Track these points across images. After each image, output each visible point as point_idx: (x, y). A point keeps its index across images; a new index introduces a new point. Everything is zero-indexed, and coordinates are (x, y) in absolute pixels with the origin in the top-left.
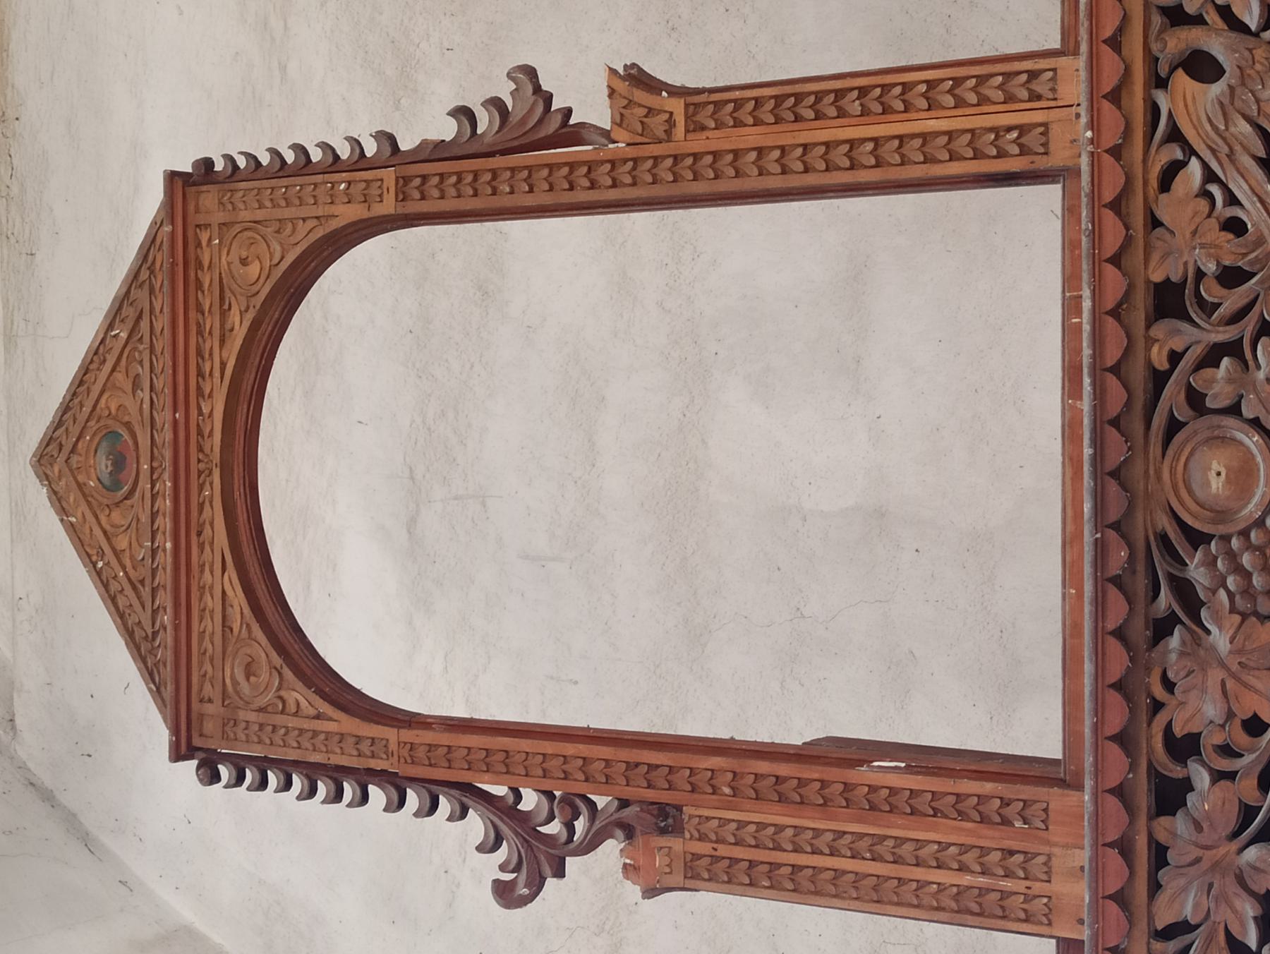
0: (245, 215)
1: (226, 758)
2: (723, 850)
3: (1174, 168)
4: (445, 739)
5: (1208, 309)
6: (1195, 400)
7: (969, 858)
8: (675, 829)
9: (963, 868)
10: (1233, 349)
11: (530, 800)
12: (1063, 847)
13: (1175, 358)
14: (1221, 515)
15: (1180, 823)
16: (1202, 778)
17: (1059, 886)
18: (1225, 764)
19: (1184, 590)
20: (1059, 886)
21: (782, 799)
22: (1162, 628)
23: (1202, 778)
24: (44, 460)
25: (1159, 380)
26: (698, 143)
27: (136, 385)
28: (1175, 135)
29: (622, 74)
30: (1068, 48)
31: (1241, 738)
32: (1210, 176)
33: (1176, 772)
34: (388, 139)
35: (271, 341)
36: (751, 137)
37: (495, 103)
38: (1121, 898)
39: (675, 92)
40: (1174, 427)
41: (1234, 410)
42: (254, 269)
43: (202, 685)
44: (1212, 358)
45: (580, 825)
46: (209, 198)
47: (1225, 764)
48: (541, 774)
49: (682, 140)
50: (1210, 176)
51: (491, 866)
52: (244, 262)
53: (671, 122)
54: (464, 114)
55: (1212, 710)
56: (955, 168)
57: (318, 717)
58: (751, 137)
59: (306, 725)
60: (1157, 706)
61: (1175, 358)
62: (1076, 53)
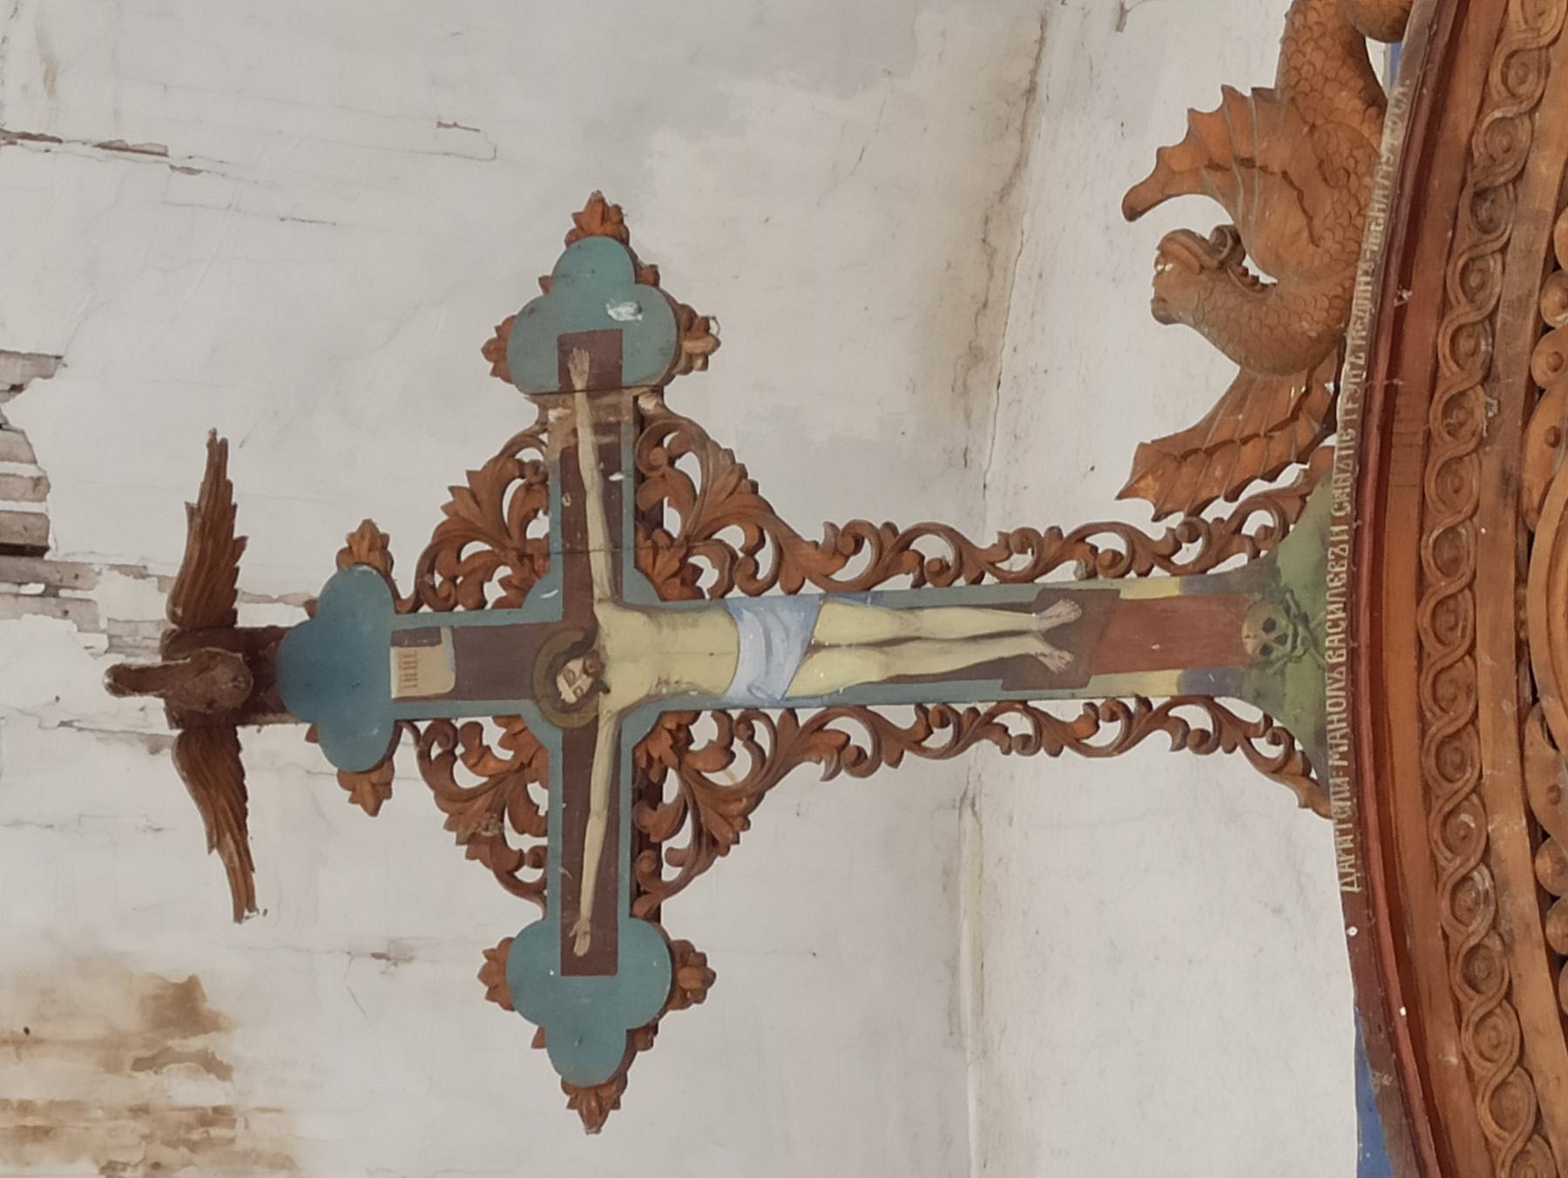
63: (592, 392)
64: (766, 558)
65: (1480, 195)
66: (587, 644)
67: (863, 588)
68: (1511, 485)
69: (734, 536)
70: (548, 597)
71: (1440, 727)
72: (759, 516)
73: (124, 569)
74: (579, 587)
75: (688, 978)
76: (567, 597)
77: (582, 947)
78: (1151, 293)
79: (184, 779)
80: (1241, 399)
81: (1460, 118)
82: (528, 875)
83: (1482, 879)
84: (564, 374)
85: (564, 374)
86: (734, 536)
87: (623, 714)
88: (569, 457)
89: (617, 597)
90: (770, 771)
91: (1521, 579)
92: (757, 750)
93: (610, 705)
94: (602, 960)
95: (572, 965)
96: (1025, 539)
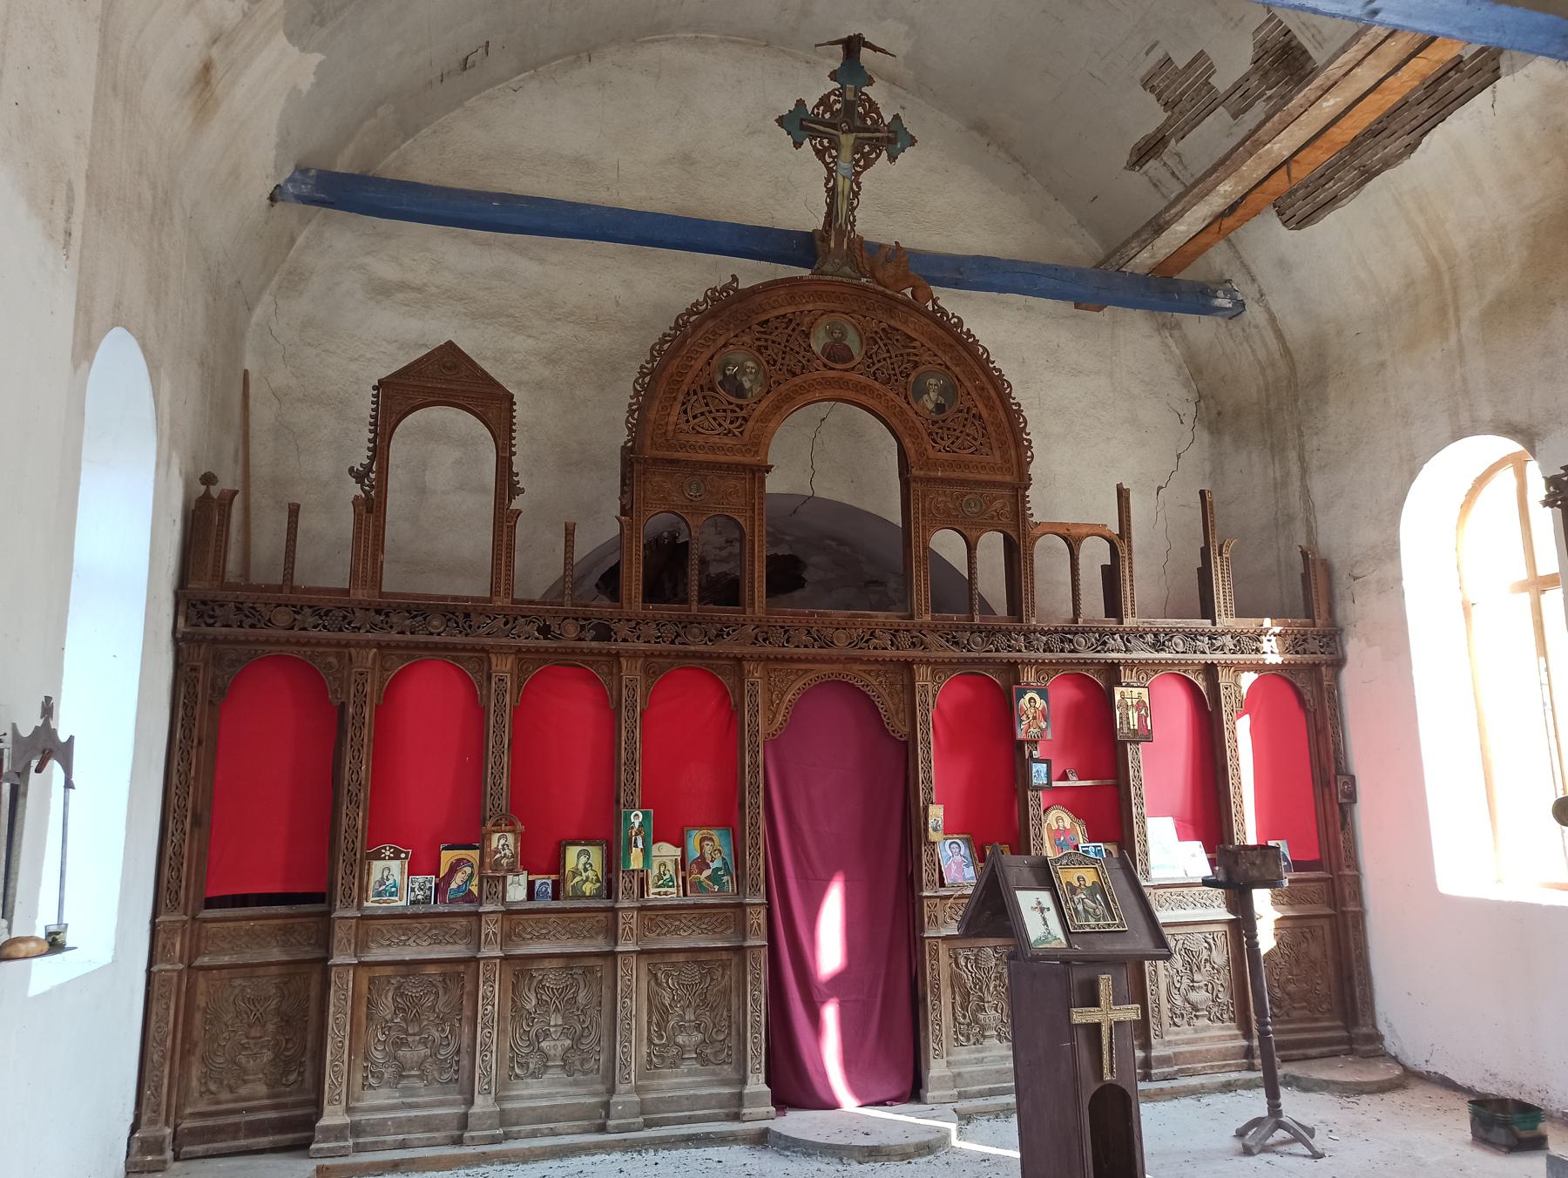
0: (502, 414)
1: (378, 406)
2: (364, 522)
3: (490, 618)
4: (385, 457)
5: (465, 622)
6: (449, 620)
7: (365, 574)
8: (367, 512)
9: (362, 573)
10: (458, 626)
11: (372, 476)
12: (1234, 247)
13: (457, 616)
14: (429, 622)
15: (374, 614)
16: (382, 618)
17: (360, 591)
18: (384, 622)
19: (416, 616)
20: (360, 591)
21: (375, 536)
22: (409, 612)
23: (382, 618)
24: (450, 344)
25: (453, 614)
26: (505, 528)
27: (467, 376)
28: (495, 618)
29: (937, 291)
30: (381, 594)
31: (389, 625)
32: (488, 624)
33: (383, 613)
34: (515, 454)
35: (193, 871)
36: (505, 539)
37: (518, 483)
38: (360, 604)
39: (515, 524)
40: (445, 616)
41: (447, 626)
42: (491, 415)
43: (413, 288)
44: (457, 623)
45: (367, 488)
46: (507, 405)
47: (384, 622)
48: (378, 478)
49: (506, 524)
50: (488, 624)
51: (357, 467)
52: (492, 413)
53: (509, 522)
54: (517, 475)
55: (394, 620)
56: (494, 579)
57: (390, 423)
58: (505, 539)
59: (388, 420)
60: (395, 611)
61: (457, 616)
62: (512, 603)
63: (888, 137)
64: (858, 169)
65: (890, 310)
66: (850, 131)
67: (852, 188)
68: (854, 311)
69: (862, 163)
70: (858, 123)
71: (824, 295)
72: (865, 168)
73: (1260, 291)
74: (859, 130)
75: (798, 145)
76: (859, 127)
77: (804, 123)
78: (1462, 607)
79: (1517, 490)
80: (1308, 535)
81: (900, 307)
82: (816, 111)
83: (804, 301)
84: (892, 132)
85: (892, 132)
86: (862, 163)
87: (838, 136)
88: (879, 131)
89: (856, 138)
90: (826, 165)
91: (957, 377)
92: (830, 163)
93: (840, 133)
94: (802, 128)
95: (802, 120)
96: (855, 220)
